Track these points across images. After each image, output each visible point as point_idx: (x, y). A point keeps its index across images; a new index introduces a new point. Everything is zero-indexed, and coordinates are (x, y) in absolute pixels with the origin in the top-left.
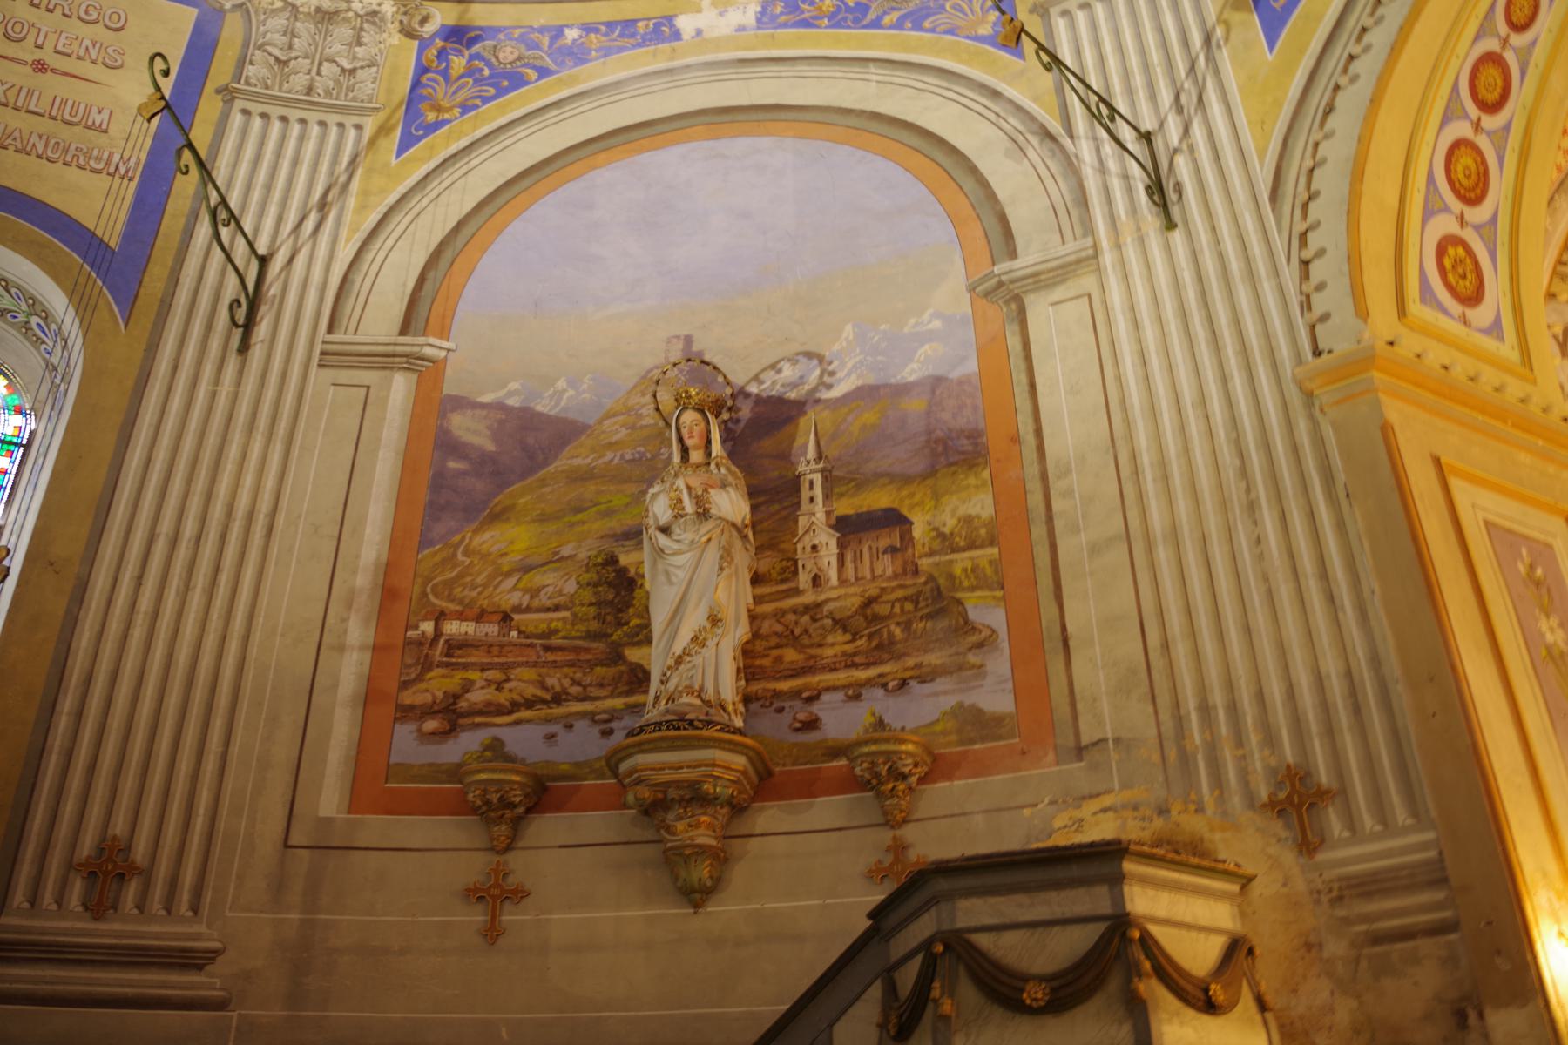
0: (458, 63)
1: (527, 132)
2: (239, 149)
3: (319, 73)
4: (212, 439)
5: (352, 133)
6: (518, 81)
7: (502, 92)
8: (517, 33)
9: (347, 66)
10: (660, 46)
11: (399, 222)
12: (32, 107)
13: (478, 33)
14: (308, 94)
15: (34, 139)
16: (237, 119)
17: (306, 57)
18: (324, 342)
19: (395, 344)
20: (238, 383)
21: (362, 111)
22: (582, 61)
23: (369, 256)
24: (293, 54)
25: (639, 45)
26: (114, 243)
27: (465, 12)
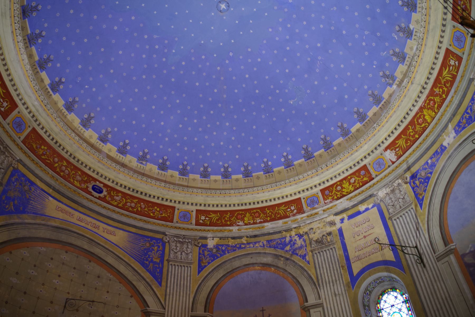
0: (417, 182)
1: (437, 188)
2: (399, 228)
3: (400, 203)
4: (431, 287)
5: (412, 210)
6: (428, 178)
7: (428, 183)
8: (421, 168)
9: (402, 197)
10: (445, 152)
11: (430, 223)
12: (369, 245)
13: (416, 174)
14: (401, 208)
15: (373, 250)
16: (395, 222)
17: (396, 201)
18: (435, 256)
19: (446, 250)
20: (428, 274)
21: (411, 205)
22: (435, 166)
23: (431, 234)
24: (394, 202)
25: (441, 155)
26: (394, 260)
27: (411, 171)
